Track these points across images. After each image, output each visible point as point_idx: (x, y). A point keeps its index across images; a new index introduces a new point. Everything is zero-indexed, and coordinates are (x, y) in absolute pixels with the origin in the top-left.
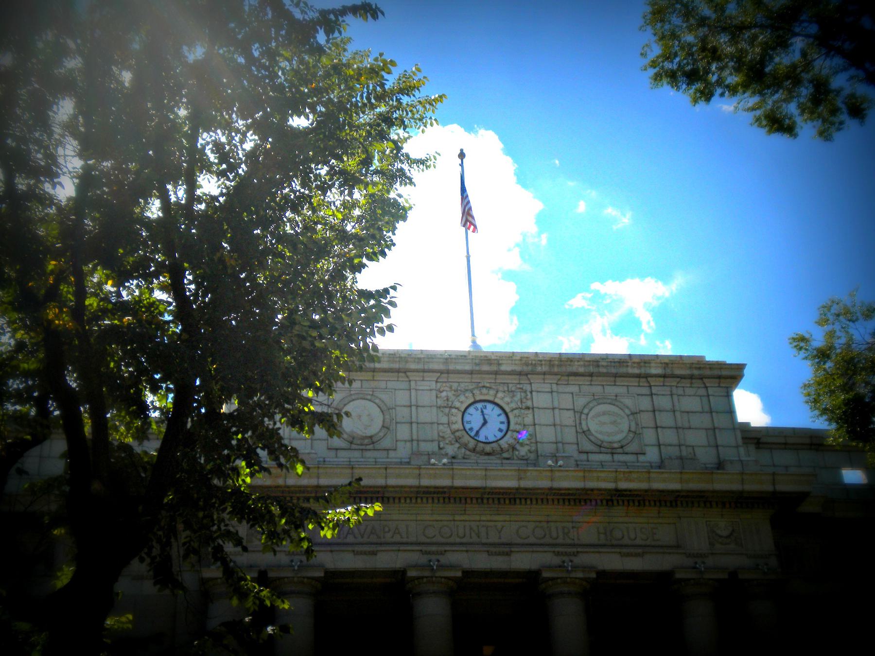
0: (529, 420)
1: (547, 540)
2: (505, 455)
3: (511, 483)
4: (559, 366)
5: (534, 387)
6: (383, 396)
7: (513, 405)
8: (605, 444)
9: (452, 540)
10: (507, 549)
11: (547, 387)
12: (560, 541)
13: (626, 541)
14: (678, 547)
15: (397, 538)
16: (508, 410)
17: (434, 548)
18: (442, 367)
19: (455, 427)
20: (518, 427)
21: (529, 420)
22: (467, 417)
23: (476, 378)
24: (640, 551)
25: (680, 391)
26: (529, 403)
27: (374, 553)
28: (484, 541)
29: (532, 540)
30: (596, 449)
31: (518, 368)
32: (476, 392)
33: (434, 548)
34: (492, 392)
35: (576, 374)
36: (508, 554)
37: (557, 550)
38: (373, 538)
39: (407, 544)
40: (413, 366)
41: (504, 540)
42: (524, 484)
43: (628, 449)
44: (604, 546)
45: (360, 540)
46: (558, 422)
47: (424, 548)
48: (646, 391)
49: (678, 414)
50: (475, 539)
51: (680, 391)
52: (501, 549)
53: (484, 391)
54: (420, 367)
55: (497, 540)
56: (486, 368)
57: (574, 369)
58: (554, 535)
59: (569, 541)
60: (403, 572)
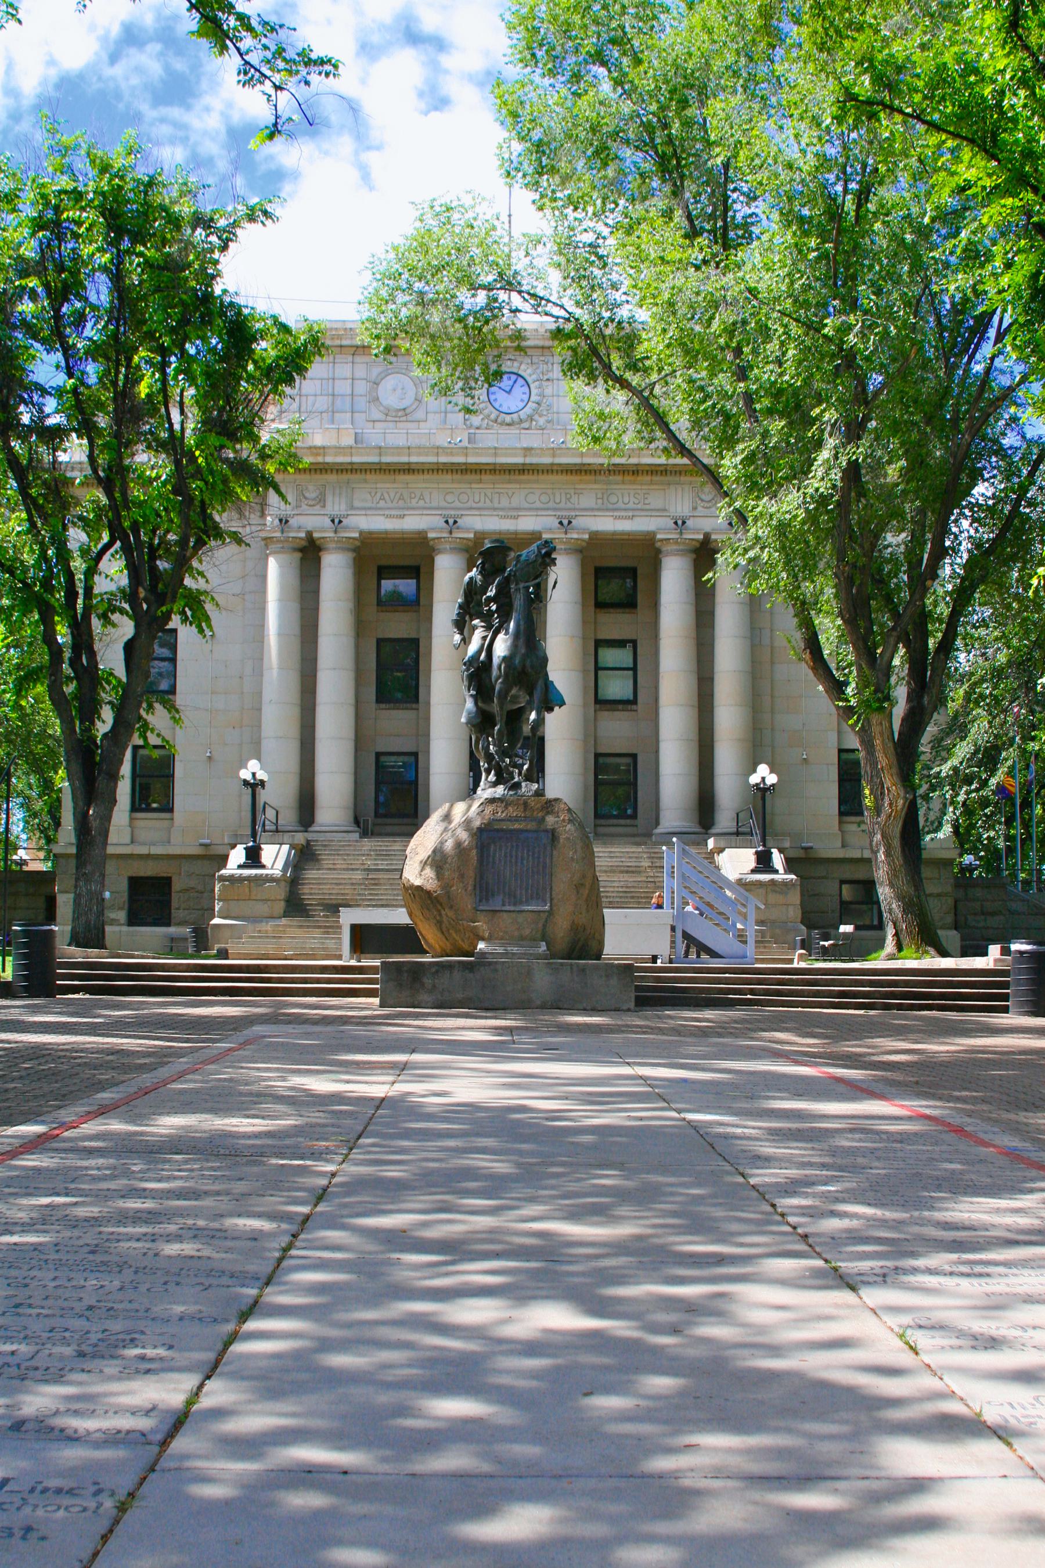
1: (551, 505)
12: (562, 505)
14: (665, 510)
16: (530, 381)
24: (630, 514)
34: (516, 364)
41: (514, 505)
44: (599, 510)
45: (390, 505)
52: (393, 512)
59: (569, 505)
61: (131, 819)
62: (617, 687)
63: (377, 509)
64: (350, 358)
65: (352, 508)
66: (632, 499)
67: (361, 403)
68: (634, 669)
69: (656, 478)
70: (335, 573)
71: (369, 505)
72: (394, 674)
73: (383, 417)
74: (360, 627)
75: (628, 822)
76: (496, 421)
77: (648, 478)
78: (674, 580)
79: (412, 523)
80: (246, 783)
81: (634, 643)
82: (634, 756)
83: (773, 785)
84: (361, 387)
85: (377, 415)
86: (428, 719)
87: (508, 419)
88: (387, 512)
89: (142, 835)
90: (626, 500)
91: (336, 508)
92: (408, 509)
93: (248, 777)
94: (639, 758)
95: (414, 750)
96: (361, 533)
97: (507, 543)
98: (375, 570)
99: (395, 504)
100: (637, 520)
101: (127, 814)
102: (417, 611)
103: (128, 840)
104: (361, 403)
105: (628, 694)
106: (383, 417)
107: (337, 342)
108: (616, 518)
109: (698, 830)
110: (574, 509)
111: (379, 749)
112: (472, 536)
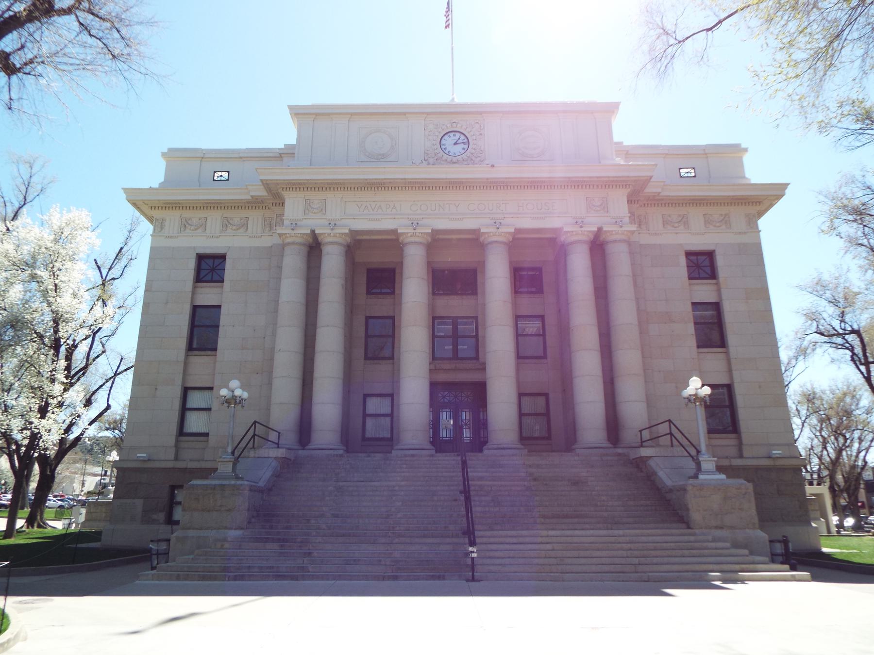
109: (611, 445)
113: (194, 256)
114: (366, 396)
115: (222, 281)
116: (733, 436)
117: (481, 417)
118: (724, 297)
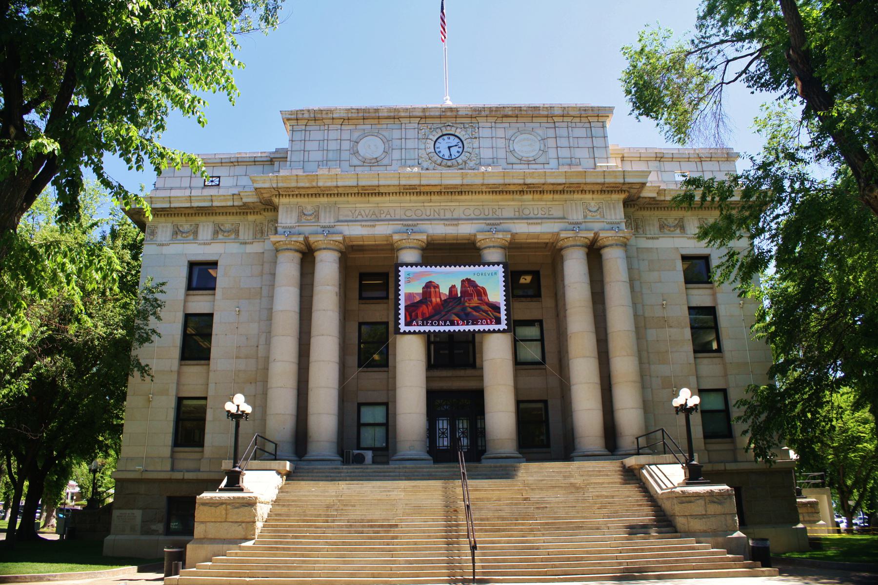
0: (476, 145)
1: (482, 216)
2: (460, 167)
3: (458, 181)
4: (496, 111)
5: (480, 125)
6: (385, 133)
7: (467, 136)
8: (524, 159)
9: (422, 217)
10: (372, 223)
11: (489, 125)
12: (490, 216)
13: (532, 215)
14: (564, 218)
15: (388, 217)
16: (463, 139)
17: (410, 222)
18: (421, 114)
19: (429, 151)
20: (470, 150)
21: (476, 145)
22: (437, 145)
23: (443, 120)
24: (540, 221)
25: (574, 125)
26: (477, 135)
27: (374, 226)
28: (442, 217)
29: (473, 216)
30: (519, 161)
31: (470, 113)
32: (443, 129)
33: (410, 222)
34: (454, 129)
35: (507, 116)
36: (457, 225)
37: (488, 222)
38: (374, 217)
39: (532, 218)
40: (403, 114)
41: (455, 217)
42: (465, 182)
43: (537, 161)
44: (517, 219)
45: (365, 218)
46: (494, 145)
47: (405, 223)
48: (552, 125)
49: (571, 139)
50: (437, 216)
51: (574, 125)
52: (369, 223)
53: (449, 128)
54: (407, 114)
55: (450, 217)
56: (449, 114)
57: (506, 113)
58: (536, 212)
59: (495, 216)
60: (558, 234)
61: (173, 452)
62: (532, 352)
63: (355, 221)
64: (339, 127)
65: (338, 221)
66: (540, 212)
67: (345, 155)
68: (542, 340)
69: (557, 196)
70: (327, 268)
71: (351, 218)
72: (369, 350)
73: (361, 164)
74: (345, 314)
75: (544, 450)
76: (440, 165)
77: (550, 196)
78: (575, 269)
79: (382, 230)
80: (230, 414)
81: (540, 322)
82: (545, 402)
83: (696, 405)
84: (346, 145)
85: (355, 162)
86: (394, 378)
87: (449, 163)
88: (363, 223)
89: (180, 465)
90: (536, 212)
91: (327, 221)
92: (378, 220)
93: (234, 410)
94: (550, 403)
95: (385, 401)
96: (344, 238)
97: (430, 466)
98: (358, 275)
99: (369, 218)
100: (544, 225)
101: (170, 449)
102: (387, 303)
103: (169, 469)
104: (345, 155)
105: (538, 357)
106: (361, 164)
107: (330, 116)
108: (529, 224)
109: (608, 453)
110: (499, 219)
111: (362, 400)
112: (425, 237)
113: (186, 264)
114: (360, 405)
115: (214, 289)
116: (728, 440)
117: (479, 426)
118: (719, 301)
